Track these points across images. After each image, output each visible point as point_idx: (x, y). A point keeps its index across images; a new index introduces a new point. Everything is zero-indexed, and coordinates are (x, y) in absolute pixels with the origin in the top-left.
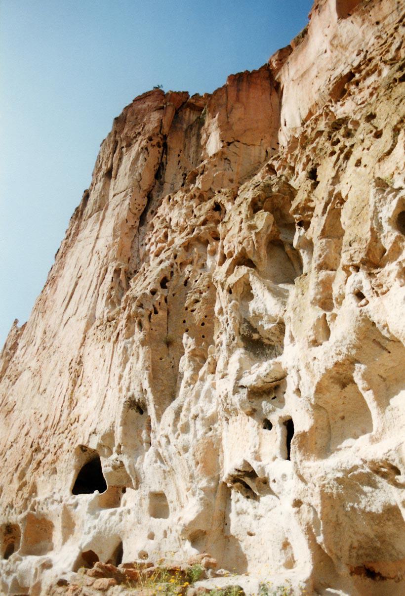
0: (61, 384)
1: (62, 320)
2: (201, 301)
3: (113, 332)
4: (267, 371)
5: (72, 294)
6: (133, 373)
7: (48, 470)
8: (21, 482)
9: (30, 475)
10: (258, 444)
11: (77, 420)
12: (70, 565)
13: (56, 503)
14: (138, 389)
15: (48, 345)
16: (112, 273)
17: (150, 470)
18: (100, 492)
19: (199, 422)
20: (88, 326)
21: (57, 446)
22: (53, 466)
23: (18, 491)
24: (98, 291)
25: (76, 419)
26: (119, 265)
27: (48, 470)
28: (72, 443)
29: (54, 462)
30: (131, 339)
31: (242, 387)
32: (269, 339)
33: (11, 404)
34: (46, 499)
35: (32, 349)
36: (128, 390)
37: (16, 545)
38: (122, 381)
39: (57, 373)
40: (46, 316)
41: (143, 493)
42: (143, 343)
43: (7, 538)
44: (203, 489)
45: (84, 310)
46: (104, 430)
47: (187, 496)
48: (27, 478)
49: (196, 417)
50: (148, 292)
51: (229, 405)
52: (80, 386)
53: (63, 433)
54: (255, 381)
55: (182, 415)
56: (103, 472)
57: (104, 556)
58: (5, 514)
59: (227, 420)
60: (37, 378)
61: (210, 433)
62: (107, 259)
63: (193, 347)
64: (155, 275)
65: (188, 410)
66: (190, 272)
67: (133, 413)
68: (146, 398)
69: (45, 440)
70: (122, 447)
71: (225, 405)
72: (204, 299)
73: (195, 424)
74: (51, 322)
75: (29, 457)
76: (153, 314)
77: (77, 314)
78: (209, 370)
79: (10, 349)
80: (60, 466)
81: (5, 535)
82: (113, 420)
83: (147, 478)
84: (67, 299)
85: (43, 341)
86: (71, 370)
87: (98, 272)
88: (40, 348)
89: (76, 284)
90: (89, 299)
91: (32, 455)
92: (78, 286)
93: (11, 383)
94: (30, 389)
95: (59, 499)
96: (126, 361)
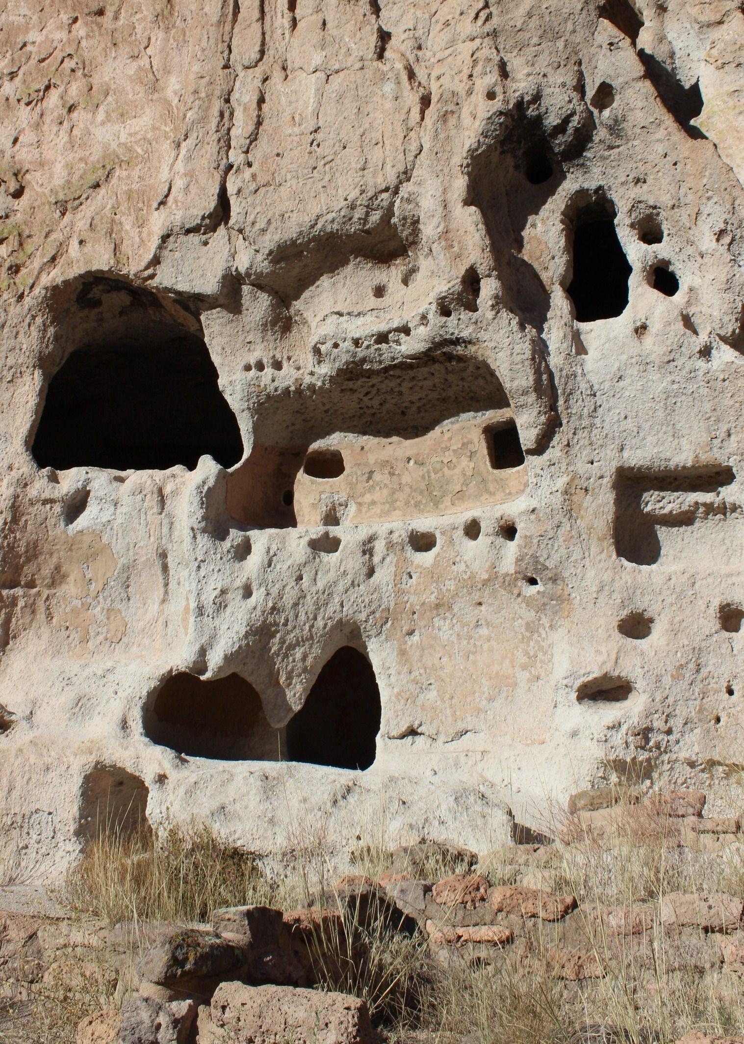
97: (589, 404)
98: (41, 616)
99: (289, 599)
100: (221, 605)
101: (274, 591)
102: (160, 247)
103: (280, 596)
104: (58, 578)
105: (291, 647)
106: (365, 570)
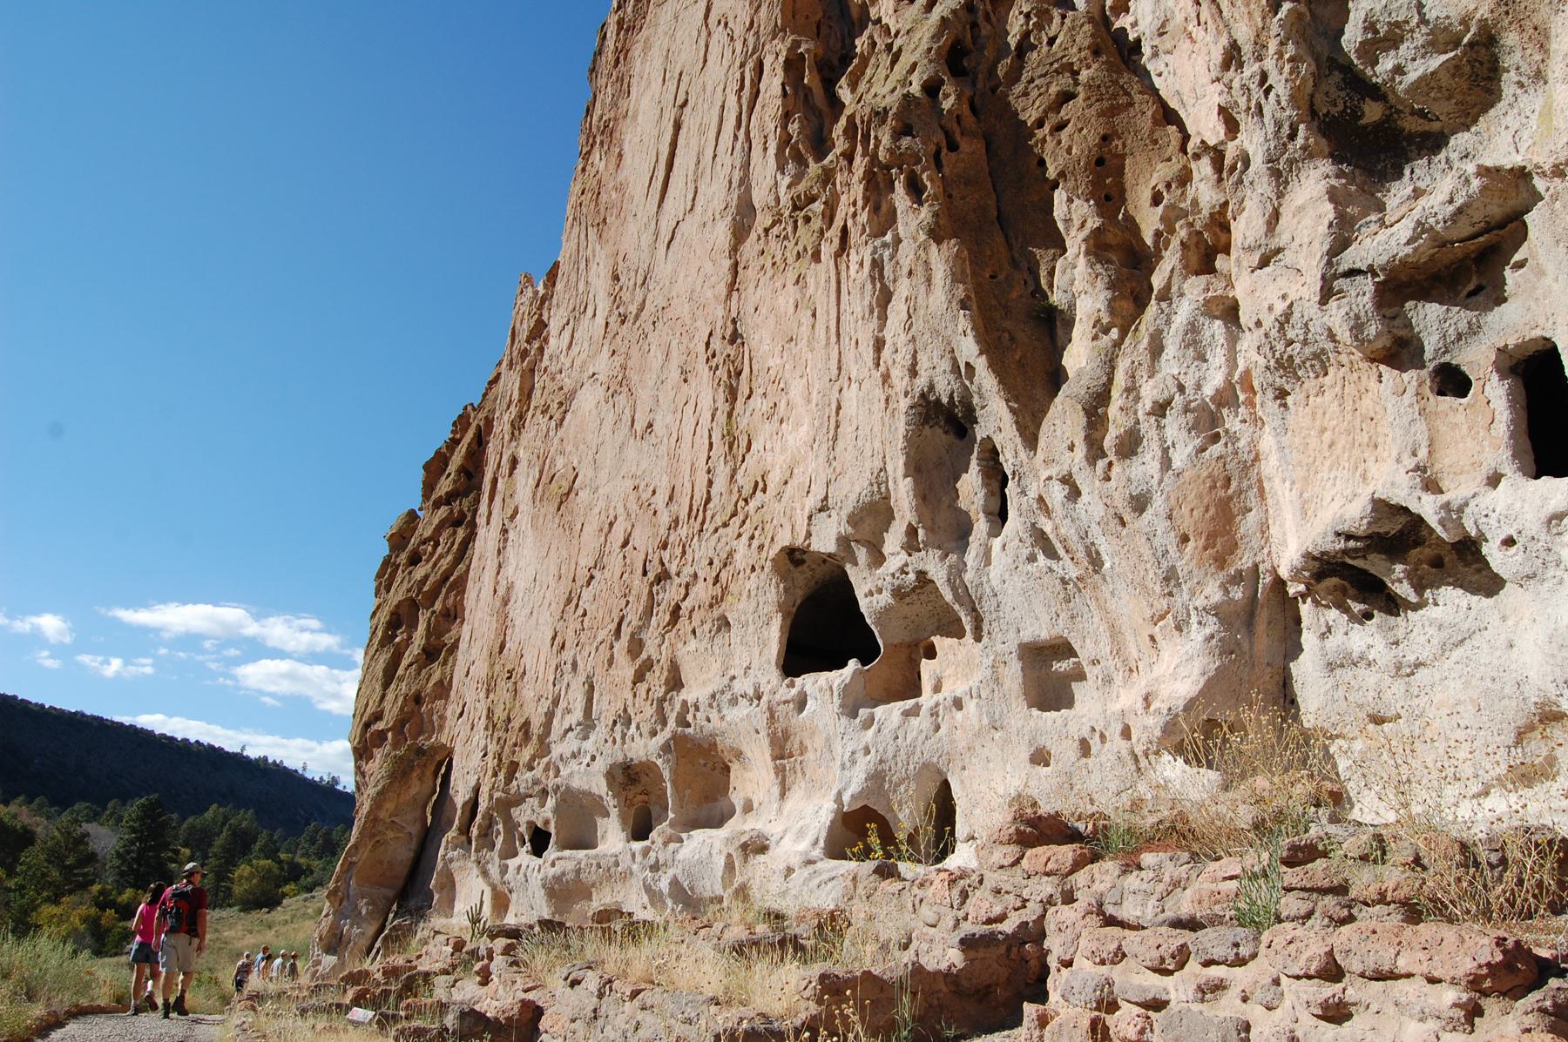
0: (692, 402)
1: (657, 234)
2: (1081, 96)
3: (822, 232)
4: (1459, 202)
5: (672, 155)
6: (918, 325)
7: (703, 623)
8: (638, 662)
9: (658, 641)
10: (1425, 443)
11: (760, 486)
12: (816, 842)
13: (743, 702)
14: (946, 365)
15: (633, 309)
16: (780, 71)
17: (1016, 583)
18: (864, 664)
19: (1174, 426)
20: (740, 233)
21: (716, 561)
22: (716, 613)
23: (635, 683)
24: (748, 133)
25: (756, 484)
26: (795, 44)
27: (703, 623)
28: (761, 547)
29: (716, 602)
30: (888, 238)
31: (1352, 273)
32: (1422, 114)
33: (563, 476)
34: (713, 696)
35: (590, 328)
36: (913, 372)
37: (655, 810)
38: (886, 353)
39: (675, 375)
40: (610, 232)
41: (999, 647)
42: (936, 234)
43: (630, 796)
44: (1216, 610)
45: (717, 194)
46: (853, 497)
47: (1152, 638)
48: (650, 649)
49: (1161, 409)
50: (915, 89)
51: (1297, 346)
52: (749, 397)
53: (725, 525)
54: (1408, 243)
55: (1113, 411)
56: (863, 610)
57: (907, 815)
58: (614, 741)
59: (1282, 394)
60: (622, 399)
61: (1216, 449)
62: (757, 33)
63: (1094, 222)
64: (928, 35)
65: (1132, 390)
66: (1028, 16)
67: (938, 436)
68: (973, 388)
69: (678, 551)
70: (921, 532)
71: (1280, 347)
72: (1089, 86)
73: (1160, 427)
74: (627, 244)
75: (644, 597)
76: (944, 151)
77: (698, 209)
78: (1186, 267)
79: (528, 341)
80: (736, 609)
81: (624, 789)
82: (878, 464)
83: (1006, 609)
84: (661, 174)
85: (616, 300)
86: (713, 363)
87: (738, 76)
88: (611, 320)
89: (678, 126)
90: (725, 159)
91: (651, 592)
92: (683, 132)
93: (553, 423)
94: (607, 428)
95: (751, 692)
96: (885, 297)
97: (994, 602)
98: (799, 774)
99: (890, 754)
100: (854, 762)
101: (881, 749)
102: (809, 525)
103: (885, 751)
104: (803, 750)
105: (898, 785)
106: (933, 727)
